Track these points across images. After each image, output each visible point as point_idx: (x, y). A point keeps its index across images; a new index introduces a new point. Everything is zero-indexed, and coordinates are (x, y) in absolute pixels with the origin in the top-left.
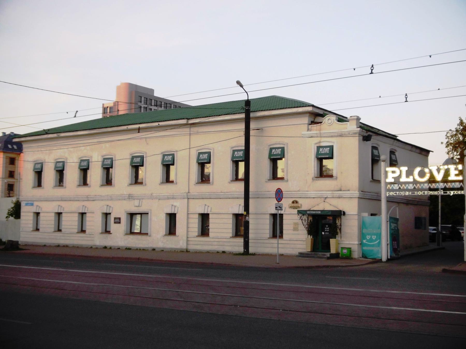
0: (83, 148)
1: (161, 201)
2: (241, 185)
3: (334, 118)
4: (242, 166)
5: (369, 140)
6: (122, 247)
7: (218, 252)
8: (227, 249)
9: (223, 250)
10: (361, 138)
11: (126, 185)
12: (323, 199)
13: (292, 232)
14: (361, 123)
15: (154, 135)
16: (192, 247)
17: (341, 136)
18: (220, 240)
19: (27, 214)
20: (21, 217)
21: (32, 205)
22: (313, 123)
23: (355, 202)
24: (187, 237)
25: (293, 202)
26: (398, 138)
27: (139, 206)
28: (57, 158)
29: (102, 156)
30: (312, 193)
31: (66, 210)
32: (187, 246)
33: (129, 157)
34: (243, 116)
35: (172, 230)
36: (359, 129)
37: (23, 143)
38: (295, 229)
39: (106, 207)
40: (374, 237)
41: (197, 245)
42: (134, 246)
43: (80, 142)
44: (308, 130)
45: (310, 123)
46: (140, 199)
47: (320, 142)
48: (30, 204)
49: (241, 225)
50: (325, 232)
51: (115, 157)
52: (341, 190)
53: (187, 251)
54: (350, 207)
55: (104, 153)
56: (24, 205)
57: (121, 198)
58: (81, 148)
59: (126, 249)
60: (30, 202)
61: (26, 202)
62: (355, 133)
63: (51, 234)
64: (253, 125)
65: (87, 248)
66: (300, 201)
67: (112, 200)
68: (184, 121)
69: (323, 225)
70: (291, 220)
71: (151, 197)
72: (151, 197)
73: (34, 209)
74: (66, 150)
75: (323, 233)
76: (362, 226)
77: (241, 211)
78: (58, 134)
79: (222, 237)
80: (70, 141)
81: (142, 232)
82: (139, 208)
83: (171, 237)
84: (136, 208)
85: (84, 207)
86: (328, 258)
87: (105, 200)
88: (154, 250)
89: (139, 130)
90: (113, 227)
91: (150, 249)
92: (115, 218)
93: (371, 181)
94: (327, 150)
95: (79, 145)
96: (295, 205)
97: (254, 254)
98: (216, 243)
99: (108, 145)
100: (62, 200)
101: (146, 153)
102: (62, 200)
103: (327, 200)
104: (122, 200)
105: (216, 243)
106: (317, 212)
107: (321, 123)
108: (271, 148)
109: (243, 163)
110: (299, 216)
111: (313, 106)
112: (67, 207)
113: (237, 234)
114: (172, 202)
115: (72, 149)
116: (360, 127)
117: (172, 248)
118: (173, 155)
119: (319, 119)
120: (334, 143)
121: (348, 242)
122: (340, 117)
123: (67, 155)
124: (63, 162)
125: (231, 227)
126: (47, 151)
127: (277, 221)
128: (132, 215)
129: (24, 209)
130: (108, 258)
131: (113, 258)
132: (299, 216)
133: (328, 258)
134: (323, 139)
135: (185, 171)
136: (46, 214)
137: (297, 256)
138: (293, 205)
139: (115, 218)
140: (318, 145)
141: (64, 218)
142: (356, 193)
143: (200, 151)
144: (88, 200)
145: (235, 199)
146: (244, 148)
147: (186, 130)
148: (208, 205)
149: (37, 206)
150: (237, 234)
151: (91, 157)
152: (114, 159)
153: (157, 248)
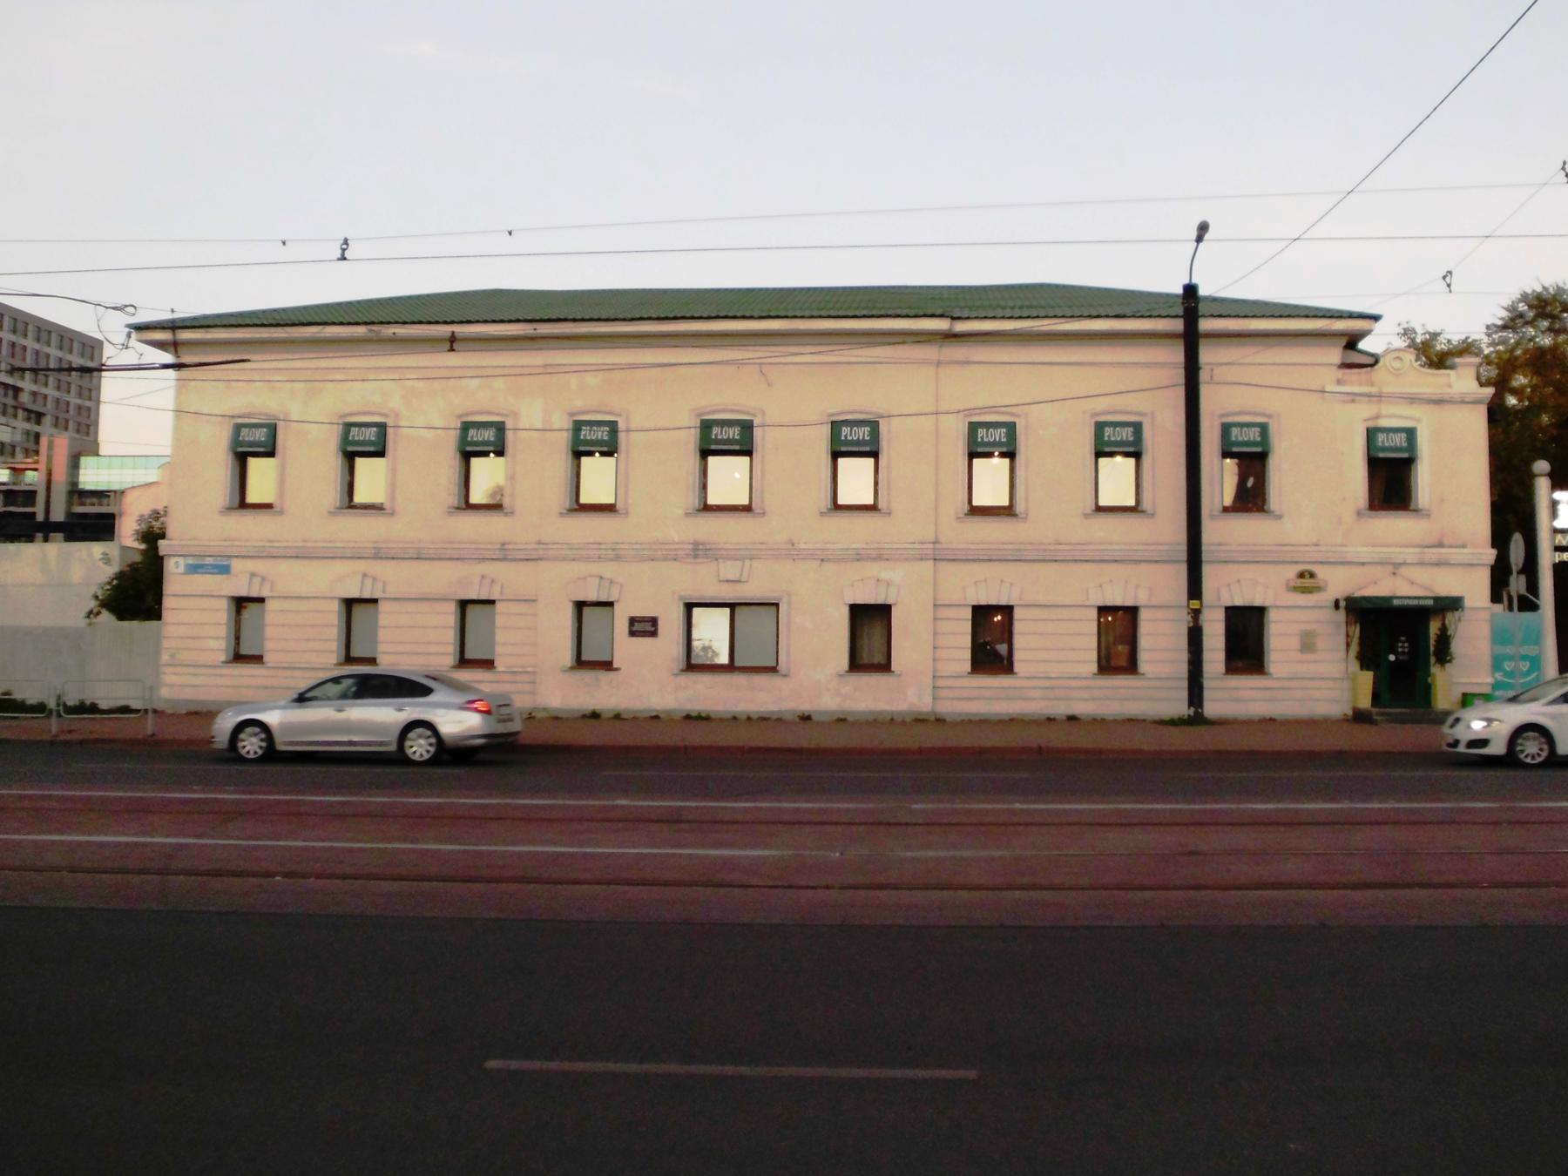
1: (828, 567)
6: (668, 712)
7: (1049, 719)
8: (1082, 708)
9: (1070, 712)
11: (681, 512)
12: (1390, 569)
13: (1299, 656)
15: (1259, 358)
16: (952, 707)
17: (1439, 402)
18: (1053, 683)
20: (165, 614)
21: (225, 570)
25: (1301, 575)
28: (349, 410)
29: (572, 415)
33: (567, 424)
38: (1307, 644)
39: (359, 578)
40: (1525, 666)
41: (969, 699)
42: (720, 708)
43: (298, 364)
46: (735, 556)
47: (1378, 417)
50: (1396, 654)
51: (628, 420)
52: (1440, 545)
53: (940, 721)
54: (1474, 587)
55: (579, 404)
56: (181, 569)
58: (464, 382)
59: (688, 717)
61: (191, 561)
62: (1476, 402)
63: (218, 671)
64: (1207, 355)
65: (1115, 721)
67: (618, 558)
69: (1397, 639)
71: (791, 552)
74: (391, 385)
75: (1392, 658)
76: (1499, 636)
78: (375, 328)
80: (273, 357)
81: (738, 663)
82: (738, 587)
87: (587, 559)
88: (806, 718)
89: (452, 342)
90: (626, 649)
91: (678, 717)
94: (260, 435)
96: (1307, 582)
97: (1221, 722)
98: (1038, 694)
99: (592, 380)
101: (763, 413)
103: (1404, 570)
104: (665, 559)
105: (1038, 694)
106: (1422, 602)
108: (576, 422)
114: (873, 569)
115: (421, 384)
117: (881, 713)
118: (1264, 428)
120: (1418, 420)
121: (1464, 680)
123: (395, 402)
124: (382, 428)
126: (297, 385)
130: (907, 752)
131: (921, 751)
134: (1386, 409)
136: (287, 605)
137: (1346, 720)
138: (1300, 582)
140: (1371, 424)
144: (504, 559)
145: (1104, 566)
148: (608, 575)
151: (516, 415)
152: (621, 426)
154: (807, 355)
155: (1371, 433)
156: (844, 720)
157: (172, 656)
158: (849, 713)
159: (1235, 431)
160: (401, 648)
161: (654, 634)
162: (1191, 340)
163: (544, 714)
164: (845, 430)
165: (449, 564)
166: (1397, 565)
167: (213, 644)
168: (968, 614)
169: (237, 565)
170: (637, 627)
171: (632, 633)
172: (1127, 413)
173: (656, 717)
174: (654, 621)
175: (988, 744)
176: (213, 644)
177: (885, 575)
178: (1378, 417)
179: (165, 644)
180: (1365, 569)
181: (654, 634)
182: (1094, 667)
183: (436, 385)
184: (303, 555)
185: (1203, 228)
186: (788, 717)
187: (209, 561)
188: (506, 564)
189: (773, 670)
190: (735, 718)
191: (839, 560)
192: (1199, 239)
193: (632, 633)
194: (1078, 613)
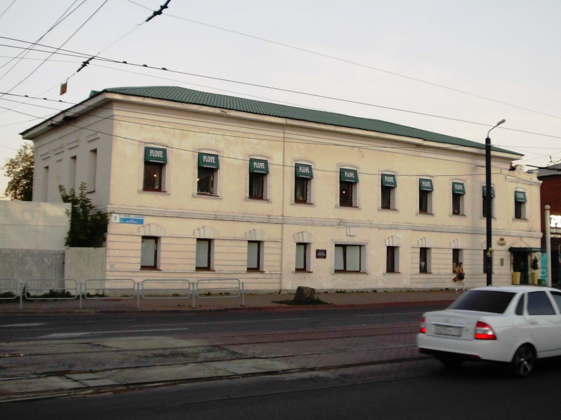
0: (255, 141)
6: (331, 290)
11: (334, 206)
13: (500, 267)
21: (141, 222)
26: (485, 185)
30: (514, 233)
35: (391, 267)
46: (356, 225)
52: (530, 231)
55: (297, 156)
56: (118, 220)
57: (325, 223)
59: (337, 292)
61: (122, 216)
64: (493, 164)
66: (505, 238)
67: (313, 224)
71: (370, 225)
72: (370, 225)
82: (353, 238)
83: (391, 276)
84: (349, 238)
87: (301, 224)
88: (375, 291)
90: (314, 262)
92: (318, 251)
95: (249, 136)
96: (502, 242)
100: (216, 219)
102: (217, 218)
103: (523, 239)
112: (399, 239)
117: (397, 288)
118: (164, 151)
124: (216, 156)
125: (265, 255)
128: (343, 247)
139: (318, 251)
143: (253, 157)
147: (278, 134)
153: (379, 289)
154: (389, 148)
155: (516, 192)
156: (387, 292)
157: (112, 266)
158: (388, 289)
159: (151, 152)
160: (229, 263)
161: (325, 257)
162: (488, 158)
163: (286, 292)
164: (255, 163)
165: (197, 220)
166: (521, 237)
167: (134, 260)
168: (418, 251)
169: (147, 220)
170: (319, 254)
171: (318, 257)
172: (351, 166)
173: (326, 292)
174: (325, 251)
175: (438, 299)
176: (134, 260)
177: (398, 235)
178: (518, 188)
179: (108, 260)
180: (515, 238)
181: (325, 257)
182: (418, 270)
183: (239, 140)
184: (180, 216)
185: (503, 121)
186: (369, 291)
187: (132, 217)
188: (268, 225)
189: (358, 272)
190: (352, 292)
191: (385, 229)
192: (499, 124)
193: (318, 257)
194: (446, 251)
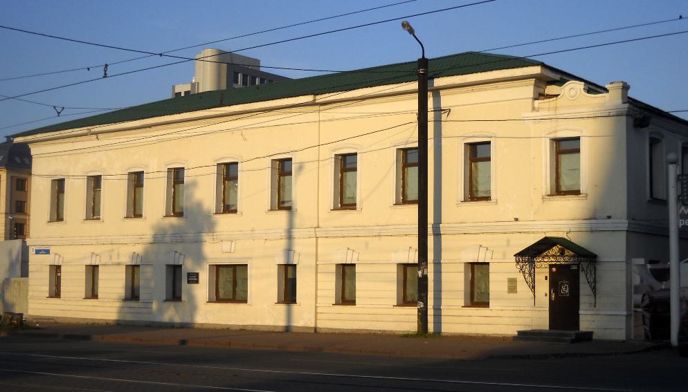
2: (414, 210)
3: (580, 86)
4: (413, 172)
5: (647, 125)
10: (631, 121)
14: (629, 98)
19: (39, 266)
20: (30, 275)
21: (47, 252)
22: (540, 96)
23: (621, 239)
24: (316, 310)
27: (230, 252)
31: (105, 260)
32: (316, 323)
34: (414, 86)
36: (627, 105)
37: (30, 146)
44: (534, 109)
45: (537, 97)
48: (45, 250)
49: (414, 285)
60: (43, 248)
68: (309, 98)
70: (504, 269)
73: (50, 260)
77: (413, 258)
79: (380, 311)
85: (94, 256)
86: (573, 341)
93: (649, 201)
105: (367, 317)
107: (557, 96)
109: (416, 168)
110: (518, 267)
111: (543, 65)
113: (404, 301)
116: (628, 102)
119: (551, 89)
122: (591, 87)
127: (477, 272)
129: (33, 259)
132: (518, 267)
133: (573, 341)
135: (313, 188)
141: (102, 275)
142: (624, 224)
146: (416, 145)
149: (56, 254)
150: (404, 301)
